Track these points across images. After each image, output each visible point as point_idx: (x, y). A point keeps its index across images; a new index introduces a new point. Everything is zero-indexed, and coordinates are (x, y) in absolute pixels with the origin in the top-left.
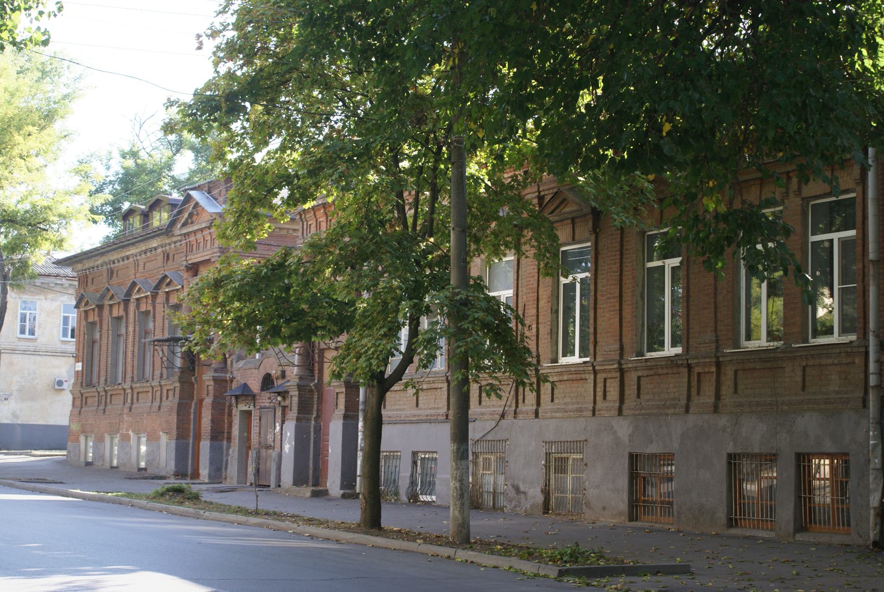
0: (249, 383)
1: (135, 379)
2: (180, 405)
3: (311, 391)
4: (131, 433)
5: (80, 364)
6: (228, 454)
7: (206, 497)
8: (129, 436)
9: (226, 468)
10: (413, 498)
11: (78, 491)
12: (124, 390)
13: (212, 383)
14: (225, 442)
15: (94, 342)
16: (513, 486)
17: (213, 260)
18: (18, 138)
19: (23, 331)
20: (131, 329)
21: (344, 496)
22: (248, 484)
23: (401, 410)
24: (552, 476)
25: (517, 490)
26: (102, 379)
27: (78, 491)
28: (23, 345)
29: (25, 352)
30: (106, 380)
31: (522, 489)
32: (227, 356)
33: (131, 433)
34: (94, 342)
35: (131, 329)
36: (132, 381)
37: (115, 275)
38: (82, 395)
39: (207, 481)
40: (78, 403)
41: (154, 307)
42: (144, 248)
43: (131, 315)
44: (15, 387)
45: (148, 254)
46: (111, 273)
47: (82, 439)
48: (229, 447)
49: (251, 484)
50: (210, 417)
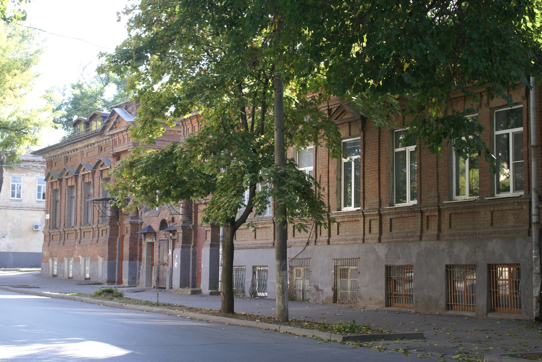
0: (152, 225)
1: (83, 224)
2: (110, 239)
3: (190, 230)
4: (80, 257)
5: (48, 215)
6: (140, 269)
7: (126, 295)
8: (79, 258)
9: (139, 277)
10: (254, 294)
11: (48, 292)
12: (76, 230)
13: (129, 225)
14: (138, 262)
15: (57, 201)
16: (315, 286)
17: (129, 150)
18: (8, 77)
19: (13, 195)
20: (79, 193)
21: (211, 294)
22: (153, 287)
23: (246, 241)
24: (339, 280)
25: (317, 289)
26: (62, 224)
27: (48, 292)
28: (13, 204)
29: (14, 208)
30: (64, 225)
31: (320, 288)
32: (139, 209)
33: (80, 257)
34: (57, 201)
35: (79, 193)
36: (81, 225)
37: (69, 160)
38: (50, 234)
39: (127, 285)
40: (48, 239)
41: (93, 180)
42: (86, 144)
43: (79, 185)
44: (9, 230)
45: (89, 147)
46: (67, 159)
47: (50, 261)
48: (140, 265)
49: (154, 287)
50: (128, 247)
